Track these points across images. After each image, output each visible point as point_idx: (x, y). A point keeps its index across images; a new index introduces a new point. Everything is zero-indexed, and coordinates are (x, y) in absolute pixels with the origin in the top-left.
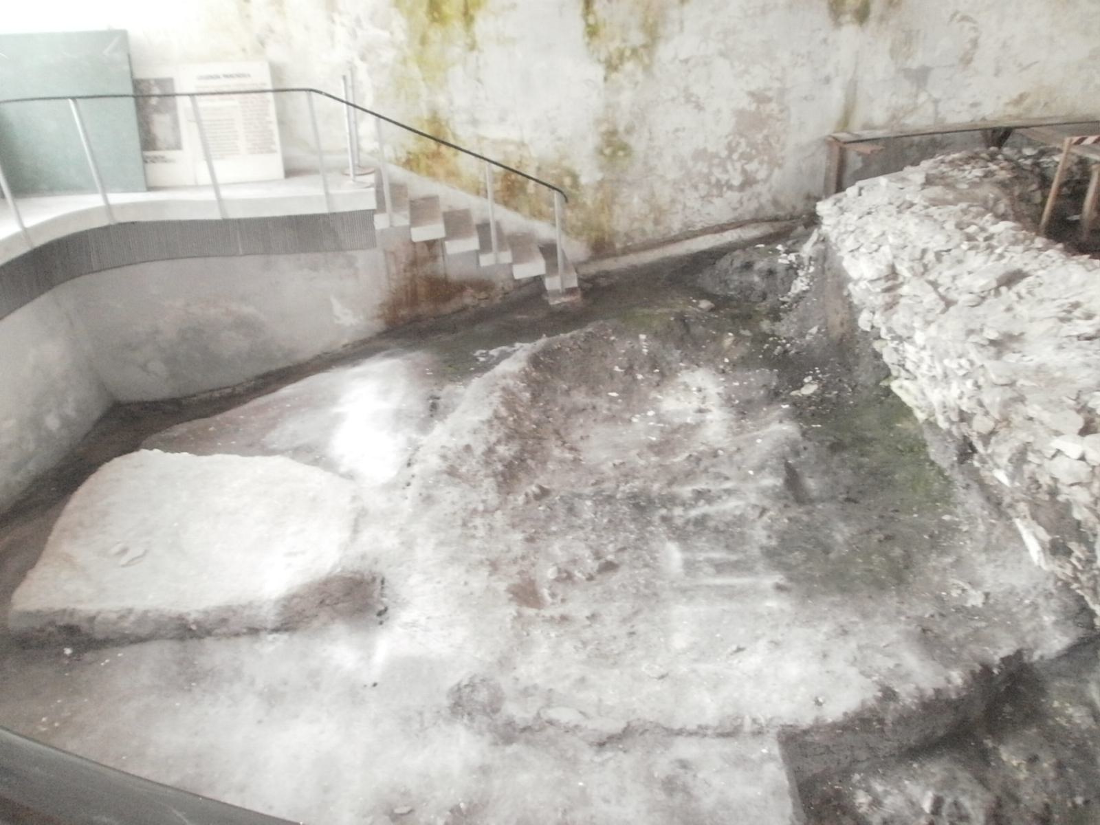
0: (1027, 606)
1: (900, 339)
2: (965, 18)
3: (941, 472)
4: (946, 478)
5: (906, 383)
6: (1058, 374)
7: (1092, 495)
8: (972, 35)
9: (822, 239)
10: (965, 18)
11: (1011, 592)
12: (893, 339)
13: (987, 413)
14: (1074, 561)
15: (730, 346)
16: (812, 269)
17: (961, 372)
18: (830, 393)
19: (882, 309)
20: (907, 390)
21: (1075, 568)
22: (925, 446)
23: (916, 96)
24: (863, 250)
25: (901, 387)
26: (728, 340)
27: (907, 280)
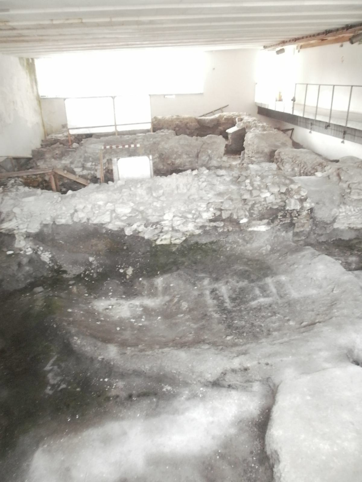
0: (274, 239)
1: (157, 223)
3: (212, 243)
4: (215, 242)
5: (163, 237)
12: (152, 226)
13: (226, 210)
18: (137, 266)
20: (165, 239)
25: (162, 240)
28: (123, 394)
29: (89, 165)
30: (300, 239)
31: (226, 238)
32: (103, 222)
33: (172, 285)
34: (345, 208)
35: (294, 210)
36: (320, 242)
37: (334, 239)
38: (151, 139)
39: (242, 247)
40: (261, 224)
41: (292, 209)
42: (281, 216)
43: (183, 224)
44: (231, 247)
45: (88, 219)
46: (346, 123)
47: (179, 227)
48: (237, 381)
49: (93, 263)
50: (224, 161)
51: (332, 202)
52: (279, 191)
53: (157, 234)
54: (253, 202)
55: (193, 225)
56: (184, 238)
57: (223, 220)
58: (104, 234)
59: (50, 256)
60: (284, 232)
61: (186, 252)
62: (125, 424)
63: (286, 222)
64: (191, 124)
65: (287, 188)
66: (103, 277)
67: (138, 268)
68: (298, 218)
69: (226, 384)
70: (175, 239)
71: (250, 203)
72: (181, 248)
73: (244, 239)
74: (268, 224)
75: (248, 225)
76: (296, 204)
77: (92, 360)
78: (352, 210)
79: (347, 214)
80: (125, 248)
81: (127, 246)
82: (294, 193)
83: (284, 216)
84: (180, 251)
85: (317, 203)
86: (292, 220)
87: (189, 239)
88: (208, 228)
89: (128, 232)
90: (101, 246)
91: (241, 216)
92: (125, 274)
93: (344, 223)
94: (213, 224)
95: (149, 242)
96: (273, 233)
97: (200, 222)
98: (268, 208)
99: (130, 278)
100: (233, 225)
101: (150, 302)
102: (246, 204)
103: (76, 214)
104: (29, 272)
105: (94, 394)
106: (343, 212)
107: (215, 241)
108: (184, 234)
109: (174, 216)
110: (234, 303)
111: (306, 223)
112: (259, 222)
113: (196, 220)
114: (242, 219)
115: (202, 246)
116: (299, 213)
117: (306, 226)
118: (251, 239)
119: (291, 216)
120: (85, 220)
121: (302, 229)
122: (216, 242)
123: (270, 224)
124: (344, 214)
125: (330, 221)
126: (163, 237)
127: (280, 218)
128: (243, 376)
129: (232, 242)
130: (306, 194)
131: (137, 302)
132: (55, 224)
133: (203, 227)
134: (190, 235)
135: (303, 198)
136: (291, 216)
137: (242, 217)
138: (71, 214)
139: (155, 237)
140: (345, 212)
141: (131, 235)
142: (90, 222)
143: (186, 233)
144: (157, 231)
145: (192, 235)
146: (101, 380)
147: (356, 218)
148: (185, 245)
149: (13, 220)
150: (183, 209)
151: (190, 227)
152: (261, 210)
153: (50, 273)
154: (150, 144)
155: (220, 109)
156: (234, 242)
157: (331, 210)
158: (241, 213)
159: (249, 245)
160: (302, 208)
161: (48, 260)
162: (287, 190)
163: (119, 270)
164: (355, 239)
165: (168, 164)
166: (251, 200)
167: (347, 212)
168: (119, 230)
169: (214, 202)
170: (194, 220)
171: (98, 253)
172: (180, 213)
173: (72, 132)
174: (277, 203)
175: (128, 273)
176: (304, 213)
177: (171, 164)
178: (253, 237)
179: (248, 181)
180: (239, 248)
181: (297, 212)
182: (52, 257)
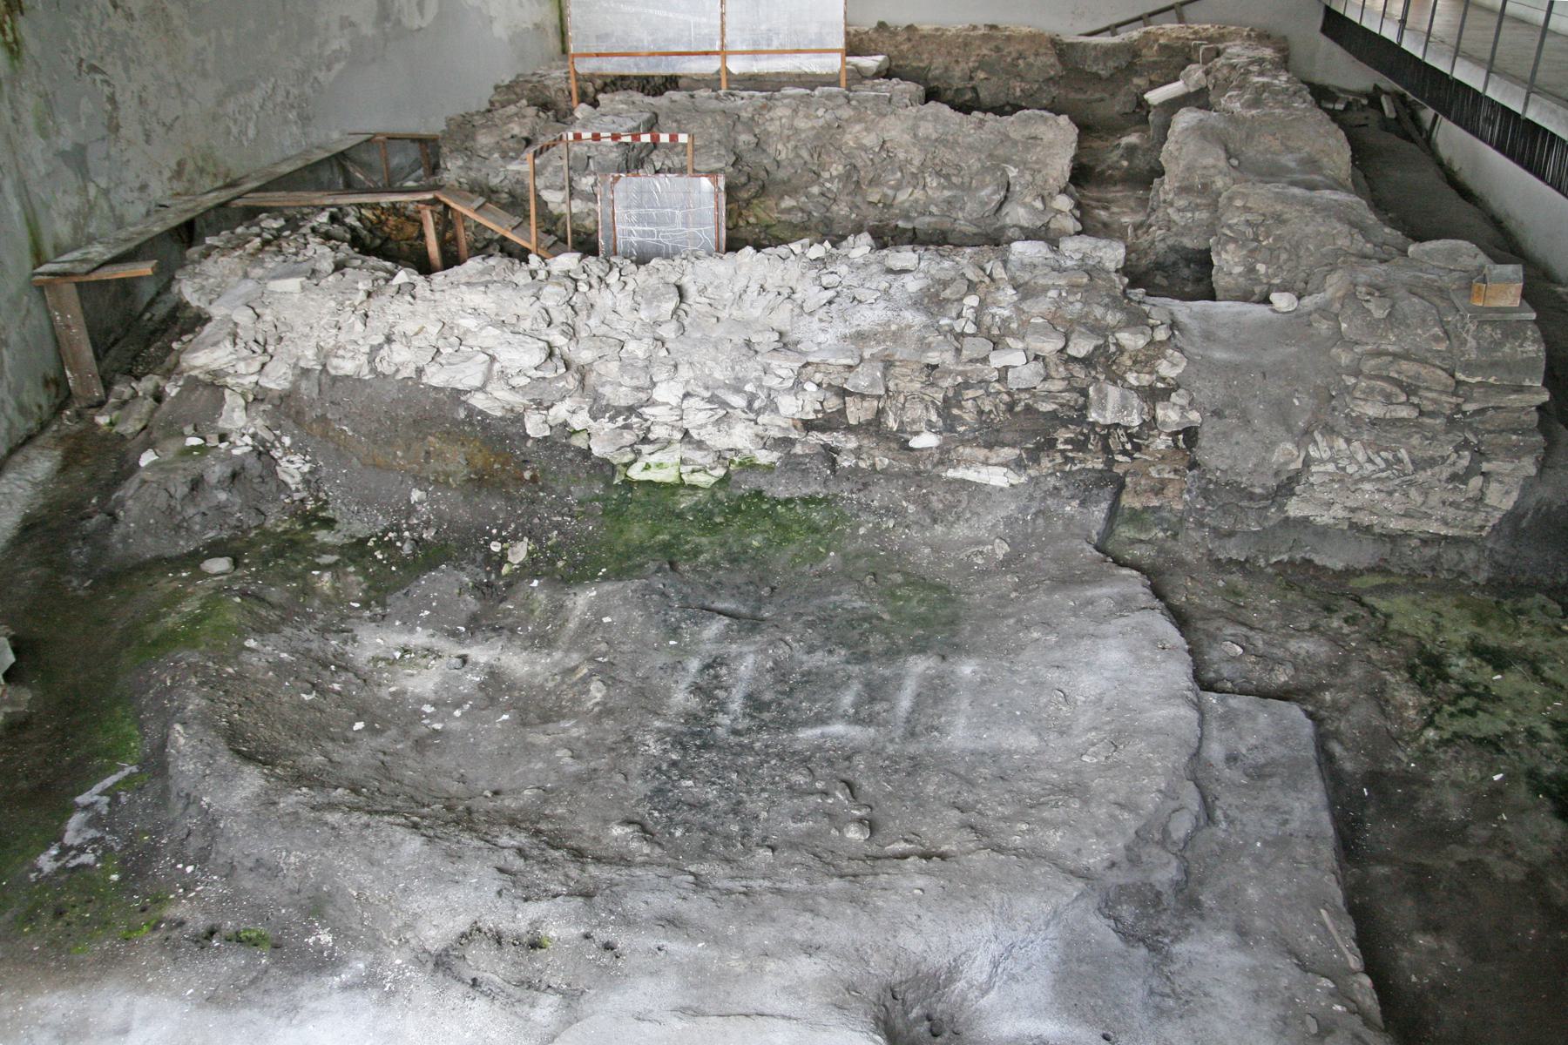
0: (1034, 520)
1: (631, 410)
2: (93, 69)
3: (808, 501)
4: (820, 502)
5: (653, 459)
6: (894, 327)
7: (1063, 379)
8: (107, 90)
9: (251, 398)
10: (93, 69)
11: (1010, 521)
12: (612, 419)
13: (863, 396)
14: (1061, 447)
15: (333, 587)
16: (287, 441)
17: (789, 383)
18: (548, 539)
19: (580, 391)
20: (660, 465)
21: (1063, 452)
22: (759, 494)
23: (85, 189)
24: (446, 351)
25: (647, 467)
26: (325, 581)
27: (566, 349)
28: (200, 922)
29: (586, 183)
30: (1143, 537)
31: (859, 490)
32: (460, 387)
33: (606, 620)
34: (1331, 448)
35: (1117, 425)
36: (1219, 560)
37: (1285, 557)
38: (820, 112)
39: (914, 533)
40: (990, 462)
41: (1109, 422)
42: (1067, 442)
43: (718, 422)
44: (877, 526)
45: (420, 371)
46: (1526, 105)
47: (703, 432)
48: (495, 973)
49: (419, 508)
50: (1060, 212)
51: (1282, 414)
52: (1062, 351)
53: (631, 446)
54: (960, 379)
55: (749, 431)
56: (720, 472)
57: (850, 429)
58: (463, 422)
59: (306, 468)
60: (1075, 503)
61: (718, 520)
62: (144, 1003)
63: (1089, 465)
64: (1031, 59)
65: (1101, 342)
66: (430, 556)
67: (548, 548)
68: (1133, 459)
69: (468, 975)
70: (693, 471)
71: (947, 382)
72: (707, 503)
73: (925, 505)
74: (1018, 465)
75: (944, 456)
76: (1124, 407)
77: (190, 800)
78: (1361, 457)
79: (1344, 469)
80: (527, 475)
81: (533, 469)
82: (1129, 363)
83: (1080, 445)
84: (701, 510)
85: (1217, 413)
86: (1110, 462)
87: (734, 478)
88: (798, 449)
89: (535, 426)
90: (456, 460)
91: (914, 422)
92: (503, 558)
93: (1331, 504)
94: (816, 438)
95: (604, 468)
96: (1031, 498)
97: (774, 424)
98: (1018, 409)
99: (512, 573)
100: (889, 449)
101: (517, 662)
102: (932, 385)
103: (385, 352)
104: (225, 507)
105: (137, 901)
106: (1322, 461)
107: (821, 496)
108: (720, 456)
109: (687, 395)
110: (753, 718)
111: (1171, 480)
112: (981, 453)
113: (758, 415)
114: (917, 433)
115: (774, 506)
116: (1137, 440)
117: (1170, 491)
118: (949, 508)
119: (1106, 449)
120: (408, 372)
121: (1155, 503)
122: (825, 499)
123: (1025, 467)
124: (1331, 467)
125: (1263, 486)
126: (653, 459)
127: (1065, 450)
128: (515, 964)
129: (881, 508)
130: (1179, 370)
131: (481, 654)
132: (327, 372)
133: (785, 443)
134: (740, 464)
135: (1160, 385)
136: (1106, 449)
137: (915, 428)
138: (372, 346)
139: (624, 454)
140: (1332, 460)
141: (545, 438)
142: (424, 380)
143: (728, 455)
144: (628, 437)
145: (750, 466)
146: (180, 866)
147: (1379, 491)
148: (721, 495)
149: (221, 345)
150: (718, 375)
151: (740, 437)
152: (991, 412)
153: (285, 521)
154: (813, 128)
155: (1171, 8)
156: (888, 509)
157: (1270, 446)
158: (916, 411)
159: (939, 529)
160: (1151, 424)
161: (298, 478)
162: (1100, 350)
163: (487, 543)
164: (1371, 570)
165: (870, 203)
166: (950, 372)
167: (1342, 463)
168: (509, 415)
169: (824, 362)
170: (752, 416)
171: (441, 479)
172: (707, 388)
173: (585, 67)
174: (1050, 395)
175: (510, 558)
176: (1161, 443)
177: (880, 205)
178: (959, 501)
179: (972, 301)
180: (901, 534)
181: (1130, 437)
182: (310, 472)
